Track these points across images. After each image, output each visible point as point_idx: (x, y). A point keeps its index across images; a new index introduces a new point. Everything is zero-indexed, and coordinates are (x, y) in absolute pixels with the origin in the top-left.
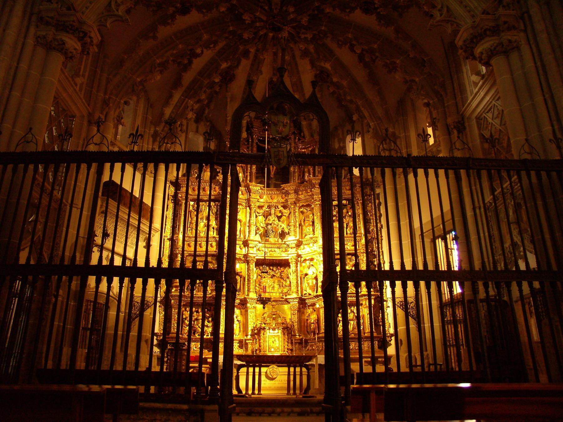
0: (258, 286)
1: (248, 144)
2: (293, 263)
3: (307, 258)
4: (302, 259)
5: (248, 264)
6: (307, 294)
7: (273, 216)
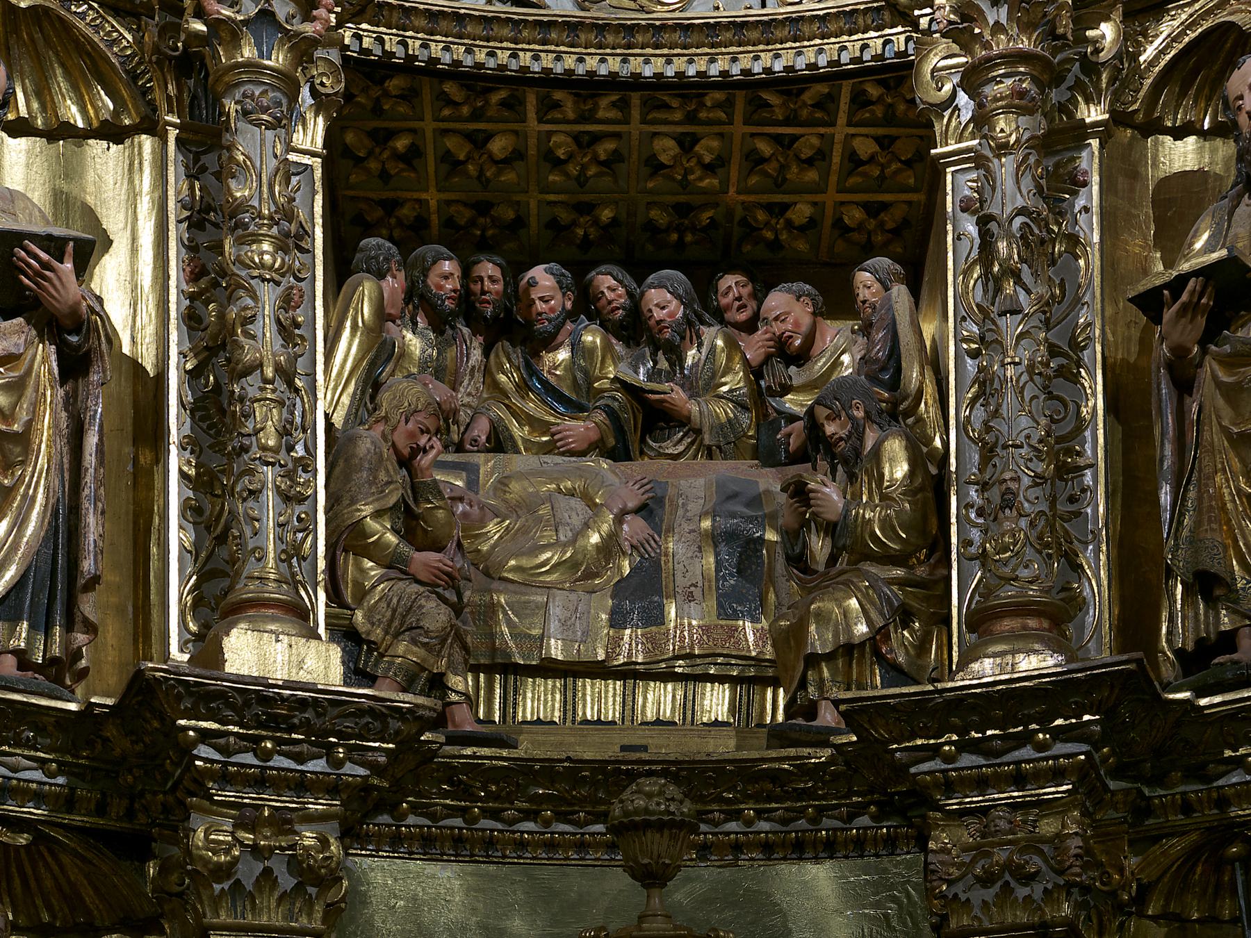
0: (385, 534)
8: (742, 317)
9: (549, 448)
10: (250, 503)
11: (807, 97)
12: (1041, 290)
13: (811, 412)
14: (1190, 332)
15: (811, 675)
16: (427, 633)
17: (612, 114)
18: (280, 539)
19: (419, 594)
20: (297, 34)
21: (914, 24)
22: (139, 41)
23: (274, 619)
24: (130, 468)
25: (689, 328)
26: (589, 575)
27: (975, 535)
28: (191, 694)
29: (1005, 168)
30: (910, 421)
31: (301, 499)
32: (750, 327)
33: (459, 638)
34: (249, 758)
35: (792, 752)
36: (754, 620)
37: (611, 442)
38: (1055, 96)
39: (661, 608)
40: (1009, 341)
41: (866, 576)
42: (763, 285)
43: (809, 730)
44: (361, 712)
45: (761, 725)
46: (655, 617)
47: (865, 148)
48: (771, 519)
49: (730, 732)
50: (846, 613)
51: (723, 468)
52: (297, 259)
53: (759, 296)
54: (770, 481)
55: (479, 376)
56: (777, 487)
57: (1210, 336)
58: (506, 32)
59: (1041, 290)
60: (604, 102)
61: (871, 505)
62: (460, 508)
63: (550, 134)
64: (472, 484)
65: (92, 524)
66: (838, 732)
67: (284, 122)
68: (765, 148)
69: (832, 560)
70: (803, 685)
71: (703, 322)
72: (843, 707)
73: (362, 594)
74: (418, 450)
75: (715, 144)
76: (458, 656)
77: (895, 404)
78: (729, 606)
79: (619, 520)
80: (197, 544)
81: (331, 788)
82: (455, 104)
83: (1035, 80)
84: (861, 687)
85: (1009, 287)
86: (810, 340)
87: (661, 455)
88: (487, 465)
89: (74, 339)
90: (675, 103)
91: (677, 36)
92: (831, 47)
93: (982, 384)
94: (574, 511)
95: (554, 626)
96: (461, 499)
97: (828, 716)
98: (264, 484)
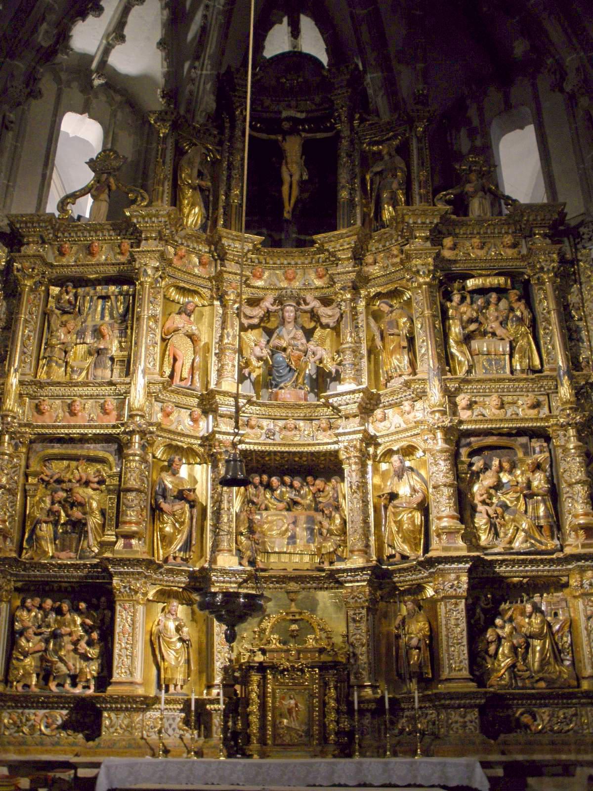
1: (222, 132)
2: (353, 460)
4: (380, 451)
6: (398, 557)
7: (290, 327)
14: (387, 502)
25: (302, 487)
42: (315, 478)
51: (308, 512)
53: (315, 479)
57: (390, 502)
64: (262, 517)
65: (194, 534)
73: (241, 543)
81: (236, 583)
88: (265, 514)
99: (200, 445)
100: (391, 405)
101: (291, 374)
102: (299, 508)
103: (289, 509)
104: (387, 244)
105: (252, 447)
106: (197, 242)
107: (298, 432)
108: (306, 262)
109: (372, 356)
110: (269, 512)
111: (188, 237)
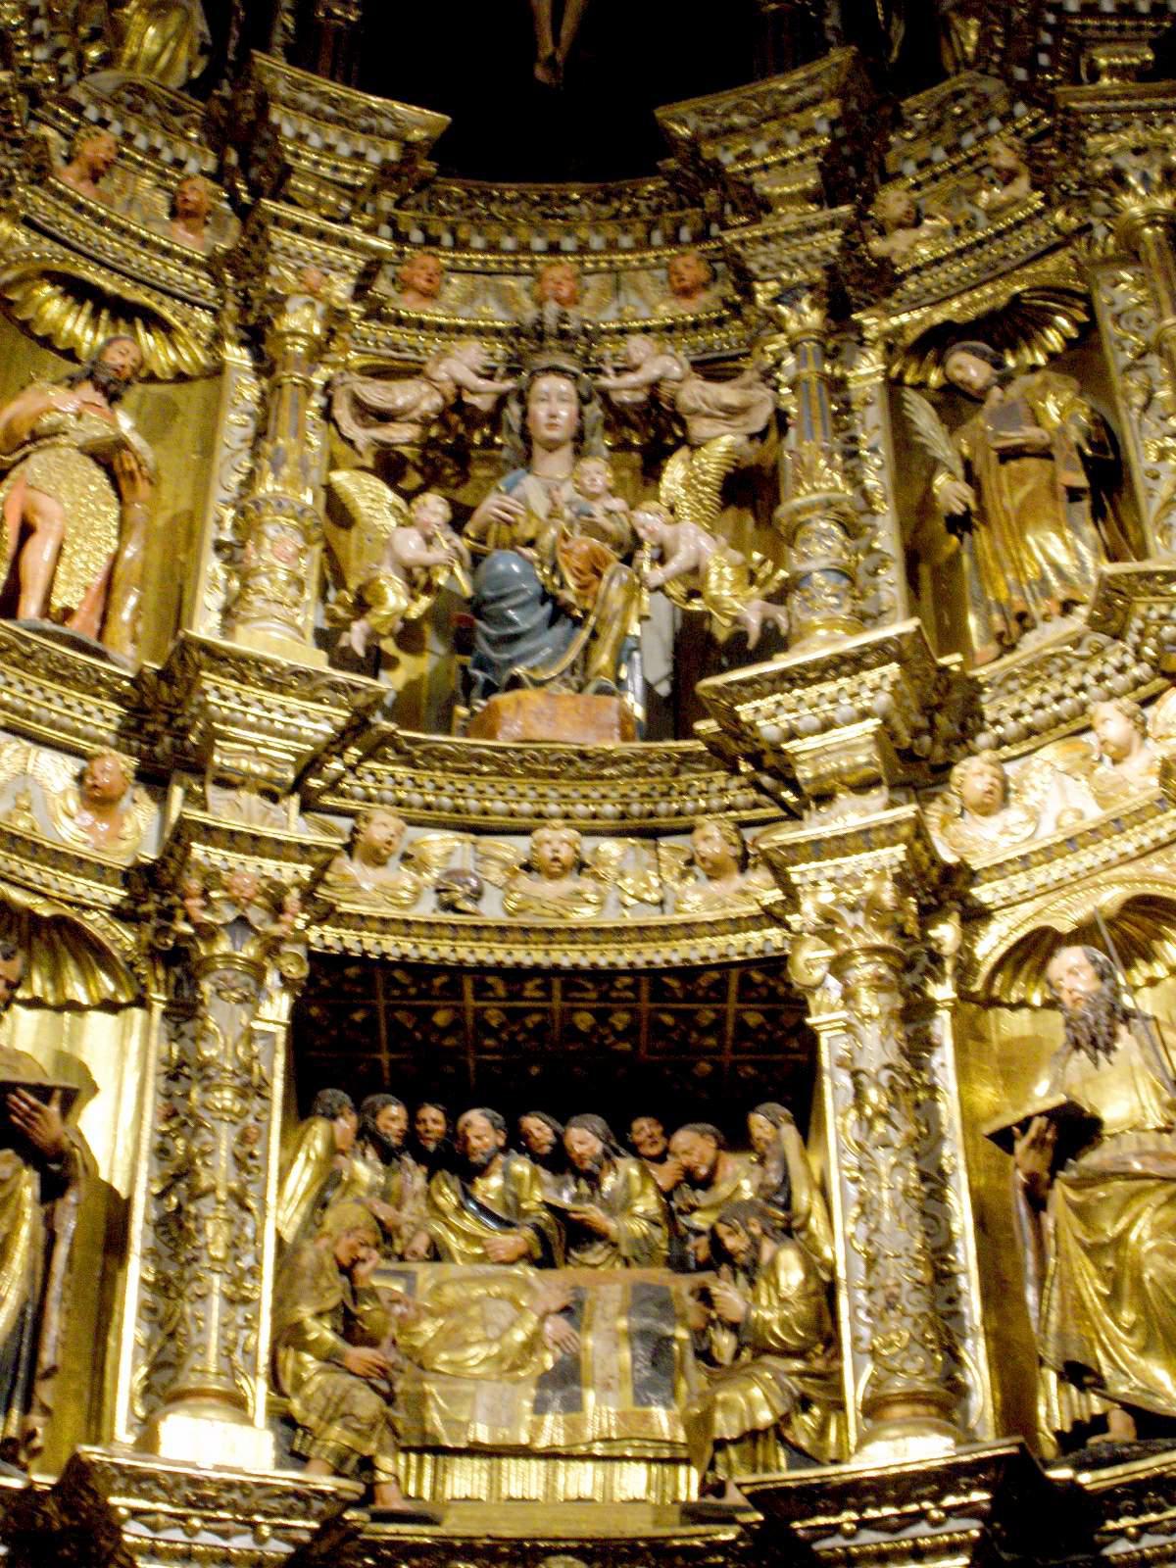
0: (322, 1332)
3: (1065, 926)
4: (991, 944)
5: (183, 1012)
6: (1120, 1427)
8: (654, 1151)
9: (482, 1259)
10: (199, 1305)
11: (703, 982)
12: (912, 1129)
13: (713, 1231)
15: (720, 1457)
16: (358, 1419)
17: (538, 994)
18: (222, 1337)
19: (353, 1386)
20: (266, 934)
21: (787, 926)
22: (139, 941)
23: (212, 1407)
24: (98, 1273)
26: (514, 1368)
27: (865, 1332)
28: (124, 1475)
29: (871, 1033)
30: (803, 1235)
31: (246, 1301)
32: (660, 1159)
33: (390, 1424)
34: (177, 1535)
35: (702, 1529)
36: (667, 1406)
37: (538, 1253)
38: (909, 979)
39: (579, 1397)
40: (884, 1169)
41: (769, 1368)
43: (717, 1508)
44: (286, 1494)
45: (675, 1502)
46: (574, 1405)
47: (753, 1019)
48: (681, 1319)
49: (647, 1508)
50: (750, 1402)
51: (637, 1273)
52: (256, 1104)
53: (669, 1133)
54: (682, 1286)
55: (421, 1200)
56: (685, 1292)
57: (1057, 1165)
58: (447, 932)
59: (912, 1129)
60: (530, 985)
61: (770, 1308)
62: (398, 1309)
63: (484, 1009)
64: (411, 1289)
65: (55, 1322)
66: (743, 1510)
67: (251, 1000)
68: (668, 1019)
69: (737, 1355)
70: (712, 1466)
71: (619, 1155)
72: (747, 1490)
73: (299, 1384)
74: (356, 1261)
75: (626, 1017)
76: (388, 1438)
77: (788, 1221)
78: (643, 1393)
79: (543, 1319)
80: (149, 1342)
82: (403, 987)
83: (891, 967)
84: (767, 1468)
85: (880, 1126)
86: (713, 1169)
87: (583, 1264)
88: (426, 1274)
89: (55, 1167)
90: (589, 986)
91: (590, 936)
92: (720, 942)
93: (862, 1205)
94: (503, 1312)
95: (481, 1412)
96: (398, 1302)
97: (734, 1497)
98: (210, 1289)
99: (119, 913)
100: (1030, 732)
101: (560, 630)
102: (596, 1254)
103: (544, 1259)
104: (968, 140)
105: (370, 943)
106: (166, 128)
107: (586, 885)
108: (626, 241)
109: (924, 571)
110: (447, 1270)
111: (134, 98)
